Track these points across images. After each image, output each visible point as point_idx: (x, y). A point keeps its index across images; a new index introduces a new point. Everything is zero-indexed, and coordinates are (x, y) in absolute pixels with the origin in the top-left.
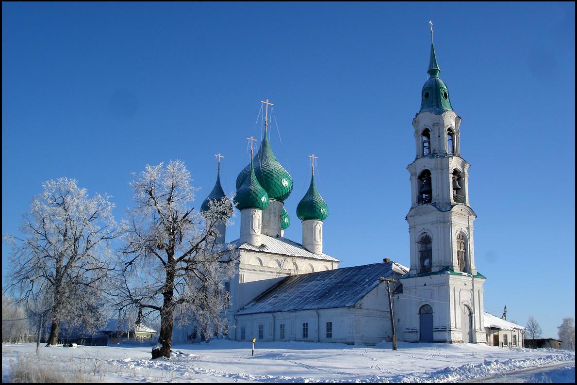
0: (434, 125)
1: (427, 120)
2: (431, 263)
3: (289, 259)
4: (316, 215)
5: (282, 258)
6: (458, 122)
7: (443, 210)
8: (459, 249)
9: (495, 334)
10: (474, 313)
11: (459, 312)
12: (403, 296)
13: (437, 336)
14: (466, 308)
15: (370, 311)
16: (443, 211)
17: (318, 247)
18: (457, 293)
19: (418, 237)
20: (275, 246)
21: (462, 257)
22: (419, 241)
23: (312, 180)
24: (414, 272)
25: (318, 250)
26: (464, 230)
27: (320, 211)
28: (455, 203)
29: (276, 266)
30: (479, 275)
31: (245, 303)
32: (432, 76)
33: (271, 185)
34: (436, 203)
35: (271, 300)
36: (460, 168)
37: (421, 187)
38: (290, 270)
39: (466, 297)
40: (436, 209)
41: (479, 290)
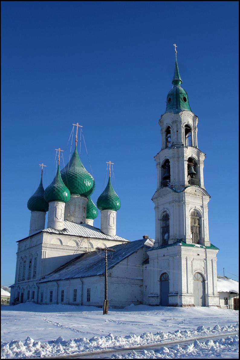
0: (173, 123)
1: (168, 119)
2: (169, 237)
3: (85, 240)
4: (110, 206)
5: (79, 239)
6: (196, 120)
7: (179, 191)
8: (193, 224)
9: (235, 297)
10: (207, 280)
11: (191, 278)
12: (149, 267)
13: (171, 300)
14: (199, 276)
15: (119, 279)
16: (178, 192)
17: (111, 230)
18: (189, 263)
19: (160, 215)
20: (74, 229)
21: (196, 231)
22: (161, 218)
23: (109, 180)
24: (157, 245)
25: (112, 233)
26: (198, 208)
27: (113, 203)
28: (189, 185)
29: (75, 245)
30: (212, 247)
31: (46, 274)
32: (176, 85)
33: (75, 184)
34: (172, 185)
35: (64, 271)
36: (195, 156)
37: (163, 173)
38: (86, 248)
39: (199, 266)
40: (172, 191)
41: (187, 257)
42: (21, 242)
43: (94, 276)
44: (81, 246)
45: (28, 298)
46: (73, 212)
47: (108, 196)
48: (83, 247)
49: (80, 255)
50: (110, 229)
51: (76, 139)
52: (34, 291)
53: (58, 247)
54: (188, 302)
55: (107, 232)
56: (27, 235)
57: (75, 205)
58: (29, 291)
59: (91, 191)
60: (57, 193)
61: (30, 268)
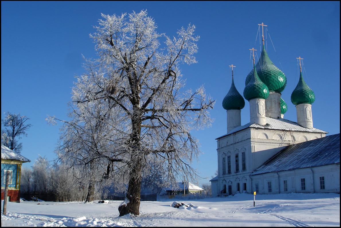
3: (288, 133)
4: (306, 100)
5: (283, 133)
17: (309, 123)
20: (276, 124)
23: (301, 75)
25: (310, 126)
27: (309, 97)
29: (279, 138)
31: (257, 167)
33: (270, 81)
38: (289, 141)
42: (220, 139)
43: (328, 165)
44: (284, 139)
45: (239, 190)
46: (270, 108)
47: (303, 90)
48: (286, 140)
49: (284, 148)
50: (308, 122)
51: (263, 38)
52: (245, 183)
53: (265, 141)
55: (306, 125)
56: (225, 133)
57: (271, 102)
58: (238, 184)
59: (283, 88)
60: (258, 90)
61: (237, 162)
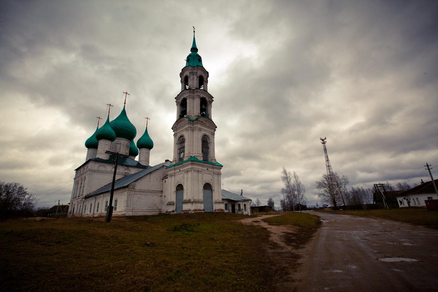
54: (199, 207)
